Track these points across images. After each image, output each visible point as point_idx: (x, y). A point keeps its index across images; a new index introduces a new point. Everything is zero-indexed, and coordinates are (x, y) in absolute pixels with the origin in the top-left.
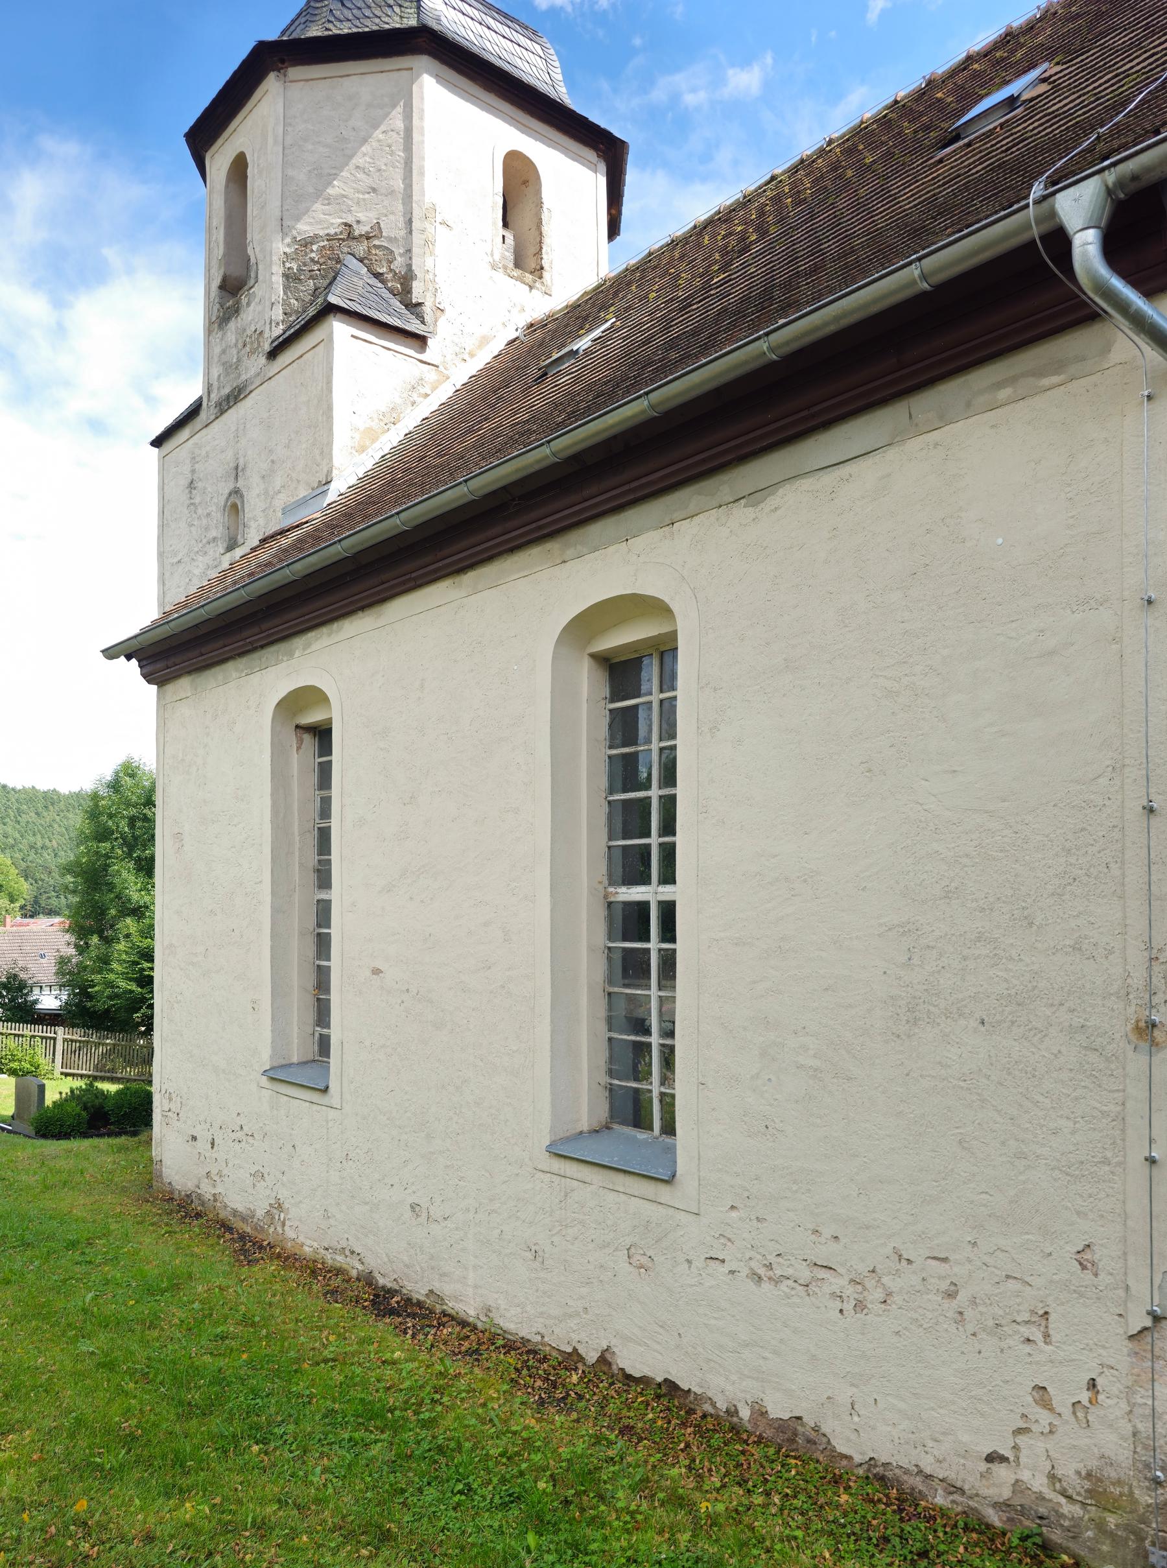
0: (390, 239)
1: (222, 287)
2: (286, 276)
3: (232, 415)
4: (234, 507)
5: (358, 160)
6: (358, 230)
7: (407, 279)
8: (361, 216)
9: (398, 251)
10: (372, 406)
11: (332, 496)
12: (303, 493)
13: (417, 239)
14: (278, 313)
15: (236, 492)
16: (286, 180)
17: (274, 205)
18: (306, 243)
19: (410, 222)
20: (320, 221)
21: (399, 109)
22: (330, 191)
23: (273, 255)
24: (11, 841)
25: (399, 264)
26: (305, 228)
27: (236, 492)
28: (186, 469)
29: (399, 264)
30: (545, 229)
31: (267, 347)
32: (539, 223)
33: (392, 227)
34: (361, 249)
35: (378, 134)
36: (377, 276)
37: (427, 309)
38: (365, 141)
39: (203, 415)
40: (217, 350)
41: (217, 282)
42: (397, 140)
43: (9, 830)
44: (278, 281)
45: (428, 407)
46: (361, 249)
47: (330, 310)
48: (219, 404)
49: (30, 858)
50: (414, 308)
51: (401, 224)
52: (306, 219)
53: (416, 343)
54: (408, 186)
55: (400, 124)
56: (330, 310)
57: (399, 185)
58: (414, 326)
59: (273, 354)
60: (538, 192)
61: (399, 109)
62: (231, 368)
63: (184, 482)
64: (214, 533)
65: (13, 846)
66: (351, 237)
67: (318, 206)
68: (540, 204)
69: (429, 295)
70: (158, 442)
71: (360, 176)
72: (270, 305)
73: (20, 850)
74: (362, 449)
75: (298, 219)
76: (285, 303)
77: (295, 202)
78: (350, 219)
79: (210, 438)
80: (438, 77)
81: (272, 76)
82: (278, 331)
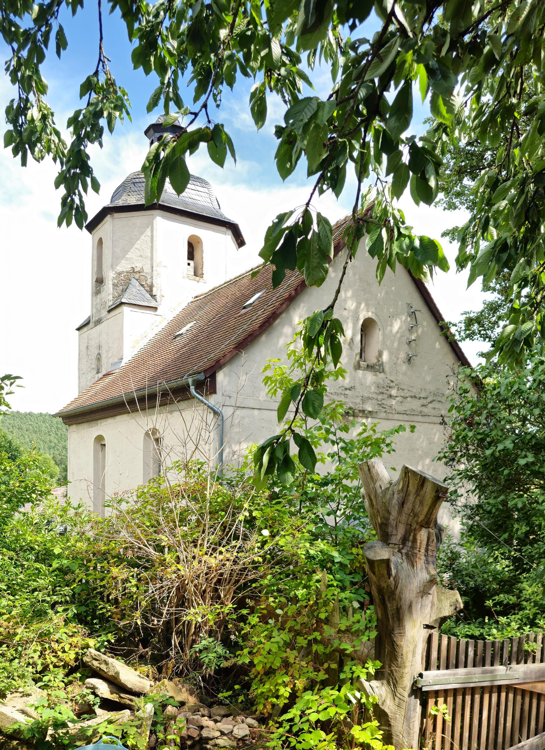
0: (146, 273)
1: (96, 281)
2: (113, 285)
3: (99, 327)
4: (99, 359)
5: (136, 246)
6: (136, 270)
7: (151, 287)
8: (137, 265)
9: (149, 277)
10: (137, 333)
11: (123, 364)
12: (116, 360)
13: (155, 273)
14: (111, 297)
15: (99, 354)
16: (113, 252)
17: (110, 260)
18: (120, 274)
19: (152, 267)
20: (124, 266)
21: (149, 229)
22: (127, 256)
23: (110, 276)
24: (53, 444)
25: (149, 282)
26: (119, 269)
27: (99, 354)
28: (86, 341)
29: (149, 282)
30: (204, 260)
31: (108, 309)
32: (202, 258)
33: (147, 269)
34: (137, 276)
35: (143, 237)
36: (142, 285)
37: (158, 297)
38: (138, 239)
39: (91, 325)
40: (95, 303)
41: (95, 280)
42: (149, 239)
43: (52, 438)
44: (111, 286)
45: (157, 330)
46: (137, 276)
47: (122, 304)
48: (95, 322)
49: (63, 454)
50: (153, 296)
51: (150, 268)
52: (119, 265)
53: (153, 309)
54: (152, 255)
55: (149, 234)
56: (122, 304)
57: (149, 254)
58: (153, 304)
59: (109, 311)
60: (202, 247)
61: (149, 229)
62: (99, 311)
63: (86, 346)
64: (93, 366)
65: (54, 447)
66: (134, 272)
67: (123, 261)
68: (202, 251)
69: (159, 292)
70: (78, 329)
71: (137, 251)
72: (109, 293)
73: (58, 450)
74: (134, 347)
75: (117, 265)
76: (113, 294)
77: (116, 260)
78: (134, 266)
79: (92, 332)
80: (163, 217)
81: (109, 216)
82: (111, 303)
